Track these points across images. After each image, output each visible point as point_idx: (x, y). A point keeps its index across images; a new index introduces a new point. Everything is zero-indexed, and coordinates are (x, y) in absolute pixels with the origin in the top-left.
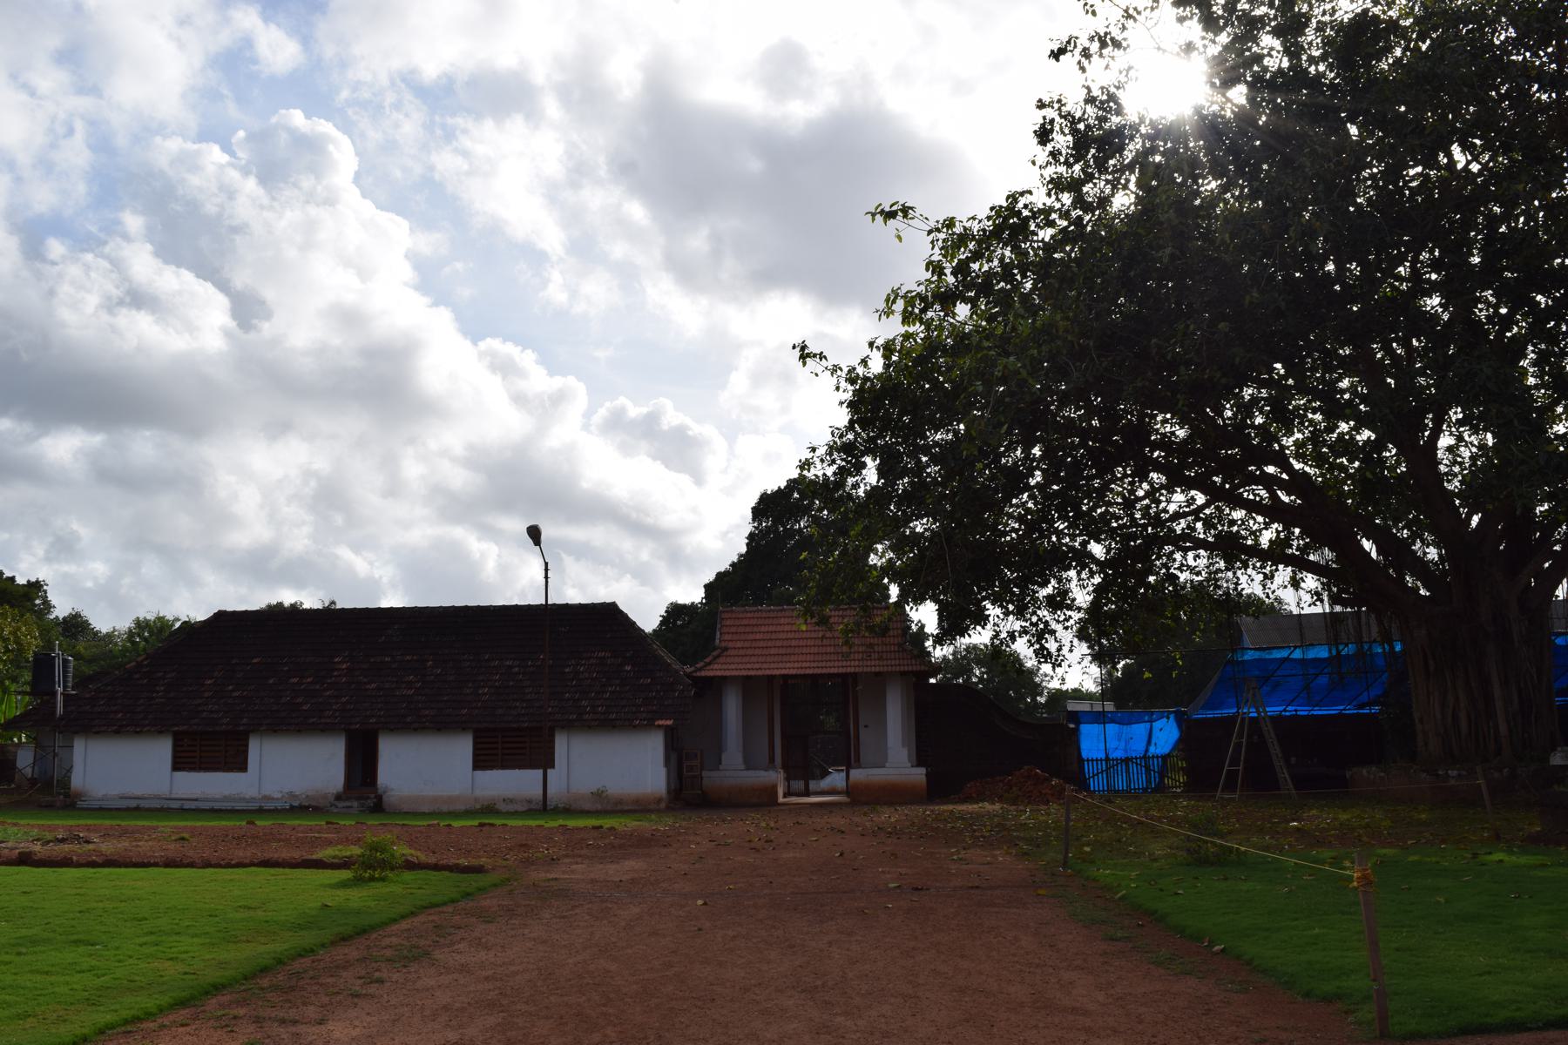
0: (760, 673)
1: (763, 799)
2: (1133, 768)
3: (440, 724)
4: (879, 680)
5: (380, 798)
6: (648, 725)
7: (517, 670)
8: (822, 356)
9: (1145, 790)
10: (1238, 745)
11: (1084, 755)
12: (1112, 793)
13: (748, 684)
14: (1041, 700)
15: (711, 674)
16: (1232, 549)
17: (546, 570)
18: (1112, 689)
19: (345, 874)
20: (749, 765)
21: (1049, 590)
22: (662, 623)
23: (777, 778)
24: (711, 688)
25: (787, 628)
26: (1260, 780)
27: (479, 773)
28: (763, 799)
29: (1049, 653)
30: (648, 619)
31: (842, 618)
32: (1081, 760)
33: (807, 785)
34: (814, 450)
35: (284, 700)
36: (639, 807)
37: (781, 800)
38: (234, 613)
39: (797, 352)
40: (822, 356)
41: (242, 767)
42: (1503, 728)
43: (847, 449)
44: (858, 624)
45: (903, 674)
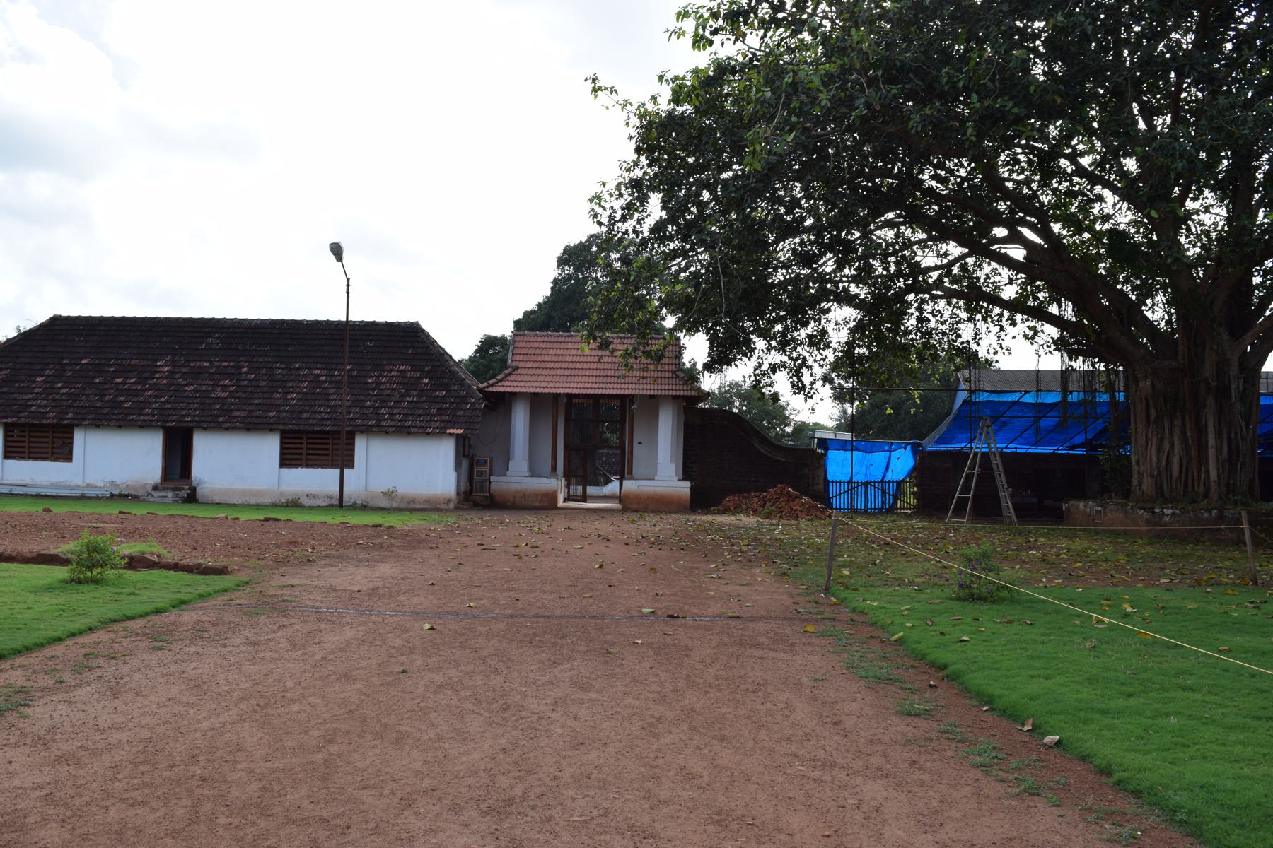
0: (546, 391)
1: (546, 503)
2: (871, 490)
3: (252, 425)
4: (653, 402)
5: (194, 490)
6: (441, 433)
7: (330, 379)
8: (612, 90)
9: (880, 510)
10: (969, 477)
11: (830, 478)
12: (854, 511)
13: (538, 402)
14: (789, 430)
15: (502, 389)
16: (977, 299)
17: (348, 285)
18: (849, 424)
19: (62, 572)
20: (534, 472)
21: (809, 330)
22: (476, 351)
23: (557, 485)
24: (500, 404)
25: (573, 352)
26: (986, 509)
27: (285, 470)
28: (546, 503)
29: (804, 387)
30: (459, 345)
31: (623, 344)
32: (826, 482)
33: (585, 491)
34: (604, 184)
35: (107, 398)
36: (430, 507)
37: (561, 503)
38: (68, 318)
39: (589, 85)
40: (612, 90)
41: (68, 457)
42: (1213, 474)
43: (635, 184)
44: (635, 349)
45: (675, 398)
